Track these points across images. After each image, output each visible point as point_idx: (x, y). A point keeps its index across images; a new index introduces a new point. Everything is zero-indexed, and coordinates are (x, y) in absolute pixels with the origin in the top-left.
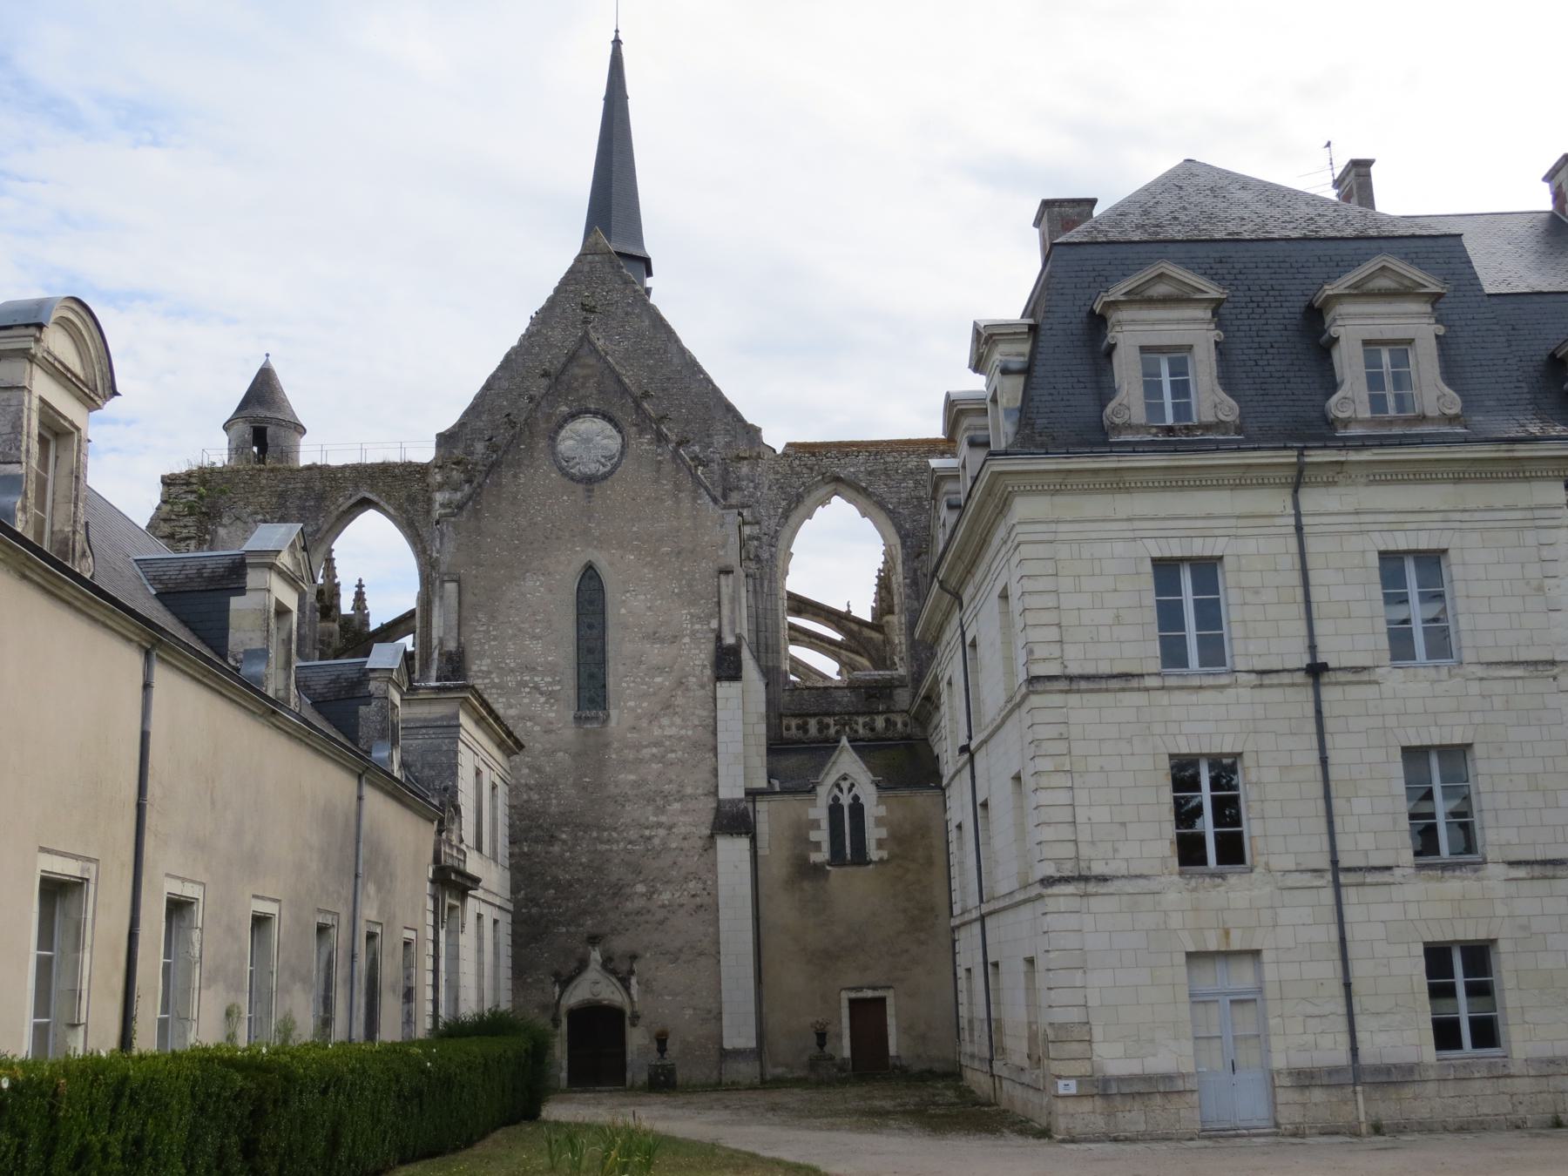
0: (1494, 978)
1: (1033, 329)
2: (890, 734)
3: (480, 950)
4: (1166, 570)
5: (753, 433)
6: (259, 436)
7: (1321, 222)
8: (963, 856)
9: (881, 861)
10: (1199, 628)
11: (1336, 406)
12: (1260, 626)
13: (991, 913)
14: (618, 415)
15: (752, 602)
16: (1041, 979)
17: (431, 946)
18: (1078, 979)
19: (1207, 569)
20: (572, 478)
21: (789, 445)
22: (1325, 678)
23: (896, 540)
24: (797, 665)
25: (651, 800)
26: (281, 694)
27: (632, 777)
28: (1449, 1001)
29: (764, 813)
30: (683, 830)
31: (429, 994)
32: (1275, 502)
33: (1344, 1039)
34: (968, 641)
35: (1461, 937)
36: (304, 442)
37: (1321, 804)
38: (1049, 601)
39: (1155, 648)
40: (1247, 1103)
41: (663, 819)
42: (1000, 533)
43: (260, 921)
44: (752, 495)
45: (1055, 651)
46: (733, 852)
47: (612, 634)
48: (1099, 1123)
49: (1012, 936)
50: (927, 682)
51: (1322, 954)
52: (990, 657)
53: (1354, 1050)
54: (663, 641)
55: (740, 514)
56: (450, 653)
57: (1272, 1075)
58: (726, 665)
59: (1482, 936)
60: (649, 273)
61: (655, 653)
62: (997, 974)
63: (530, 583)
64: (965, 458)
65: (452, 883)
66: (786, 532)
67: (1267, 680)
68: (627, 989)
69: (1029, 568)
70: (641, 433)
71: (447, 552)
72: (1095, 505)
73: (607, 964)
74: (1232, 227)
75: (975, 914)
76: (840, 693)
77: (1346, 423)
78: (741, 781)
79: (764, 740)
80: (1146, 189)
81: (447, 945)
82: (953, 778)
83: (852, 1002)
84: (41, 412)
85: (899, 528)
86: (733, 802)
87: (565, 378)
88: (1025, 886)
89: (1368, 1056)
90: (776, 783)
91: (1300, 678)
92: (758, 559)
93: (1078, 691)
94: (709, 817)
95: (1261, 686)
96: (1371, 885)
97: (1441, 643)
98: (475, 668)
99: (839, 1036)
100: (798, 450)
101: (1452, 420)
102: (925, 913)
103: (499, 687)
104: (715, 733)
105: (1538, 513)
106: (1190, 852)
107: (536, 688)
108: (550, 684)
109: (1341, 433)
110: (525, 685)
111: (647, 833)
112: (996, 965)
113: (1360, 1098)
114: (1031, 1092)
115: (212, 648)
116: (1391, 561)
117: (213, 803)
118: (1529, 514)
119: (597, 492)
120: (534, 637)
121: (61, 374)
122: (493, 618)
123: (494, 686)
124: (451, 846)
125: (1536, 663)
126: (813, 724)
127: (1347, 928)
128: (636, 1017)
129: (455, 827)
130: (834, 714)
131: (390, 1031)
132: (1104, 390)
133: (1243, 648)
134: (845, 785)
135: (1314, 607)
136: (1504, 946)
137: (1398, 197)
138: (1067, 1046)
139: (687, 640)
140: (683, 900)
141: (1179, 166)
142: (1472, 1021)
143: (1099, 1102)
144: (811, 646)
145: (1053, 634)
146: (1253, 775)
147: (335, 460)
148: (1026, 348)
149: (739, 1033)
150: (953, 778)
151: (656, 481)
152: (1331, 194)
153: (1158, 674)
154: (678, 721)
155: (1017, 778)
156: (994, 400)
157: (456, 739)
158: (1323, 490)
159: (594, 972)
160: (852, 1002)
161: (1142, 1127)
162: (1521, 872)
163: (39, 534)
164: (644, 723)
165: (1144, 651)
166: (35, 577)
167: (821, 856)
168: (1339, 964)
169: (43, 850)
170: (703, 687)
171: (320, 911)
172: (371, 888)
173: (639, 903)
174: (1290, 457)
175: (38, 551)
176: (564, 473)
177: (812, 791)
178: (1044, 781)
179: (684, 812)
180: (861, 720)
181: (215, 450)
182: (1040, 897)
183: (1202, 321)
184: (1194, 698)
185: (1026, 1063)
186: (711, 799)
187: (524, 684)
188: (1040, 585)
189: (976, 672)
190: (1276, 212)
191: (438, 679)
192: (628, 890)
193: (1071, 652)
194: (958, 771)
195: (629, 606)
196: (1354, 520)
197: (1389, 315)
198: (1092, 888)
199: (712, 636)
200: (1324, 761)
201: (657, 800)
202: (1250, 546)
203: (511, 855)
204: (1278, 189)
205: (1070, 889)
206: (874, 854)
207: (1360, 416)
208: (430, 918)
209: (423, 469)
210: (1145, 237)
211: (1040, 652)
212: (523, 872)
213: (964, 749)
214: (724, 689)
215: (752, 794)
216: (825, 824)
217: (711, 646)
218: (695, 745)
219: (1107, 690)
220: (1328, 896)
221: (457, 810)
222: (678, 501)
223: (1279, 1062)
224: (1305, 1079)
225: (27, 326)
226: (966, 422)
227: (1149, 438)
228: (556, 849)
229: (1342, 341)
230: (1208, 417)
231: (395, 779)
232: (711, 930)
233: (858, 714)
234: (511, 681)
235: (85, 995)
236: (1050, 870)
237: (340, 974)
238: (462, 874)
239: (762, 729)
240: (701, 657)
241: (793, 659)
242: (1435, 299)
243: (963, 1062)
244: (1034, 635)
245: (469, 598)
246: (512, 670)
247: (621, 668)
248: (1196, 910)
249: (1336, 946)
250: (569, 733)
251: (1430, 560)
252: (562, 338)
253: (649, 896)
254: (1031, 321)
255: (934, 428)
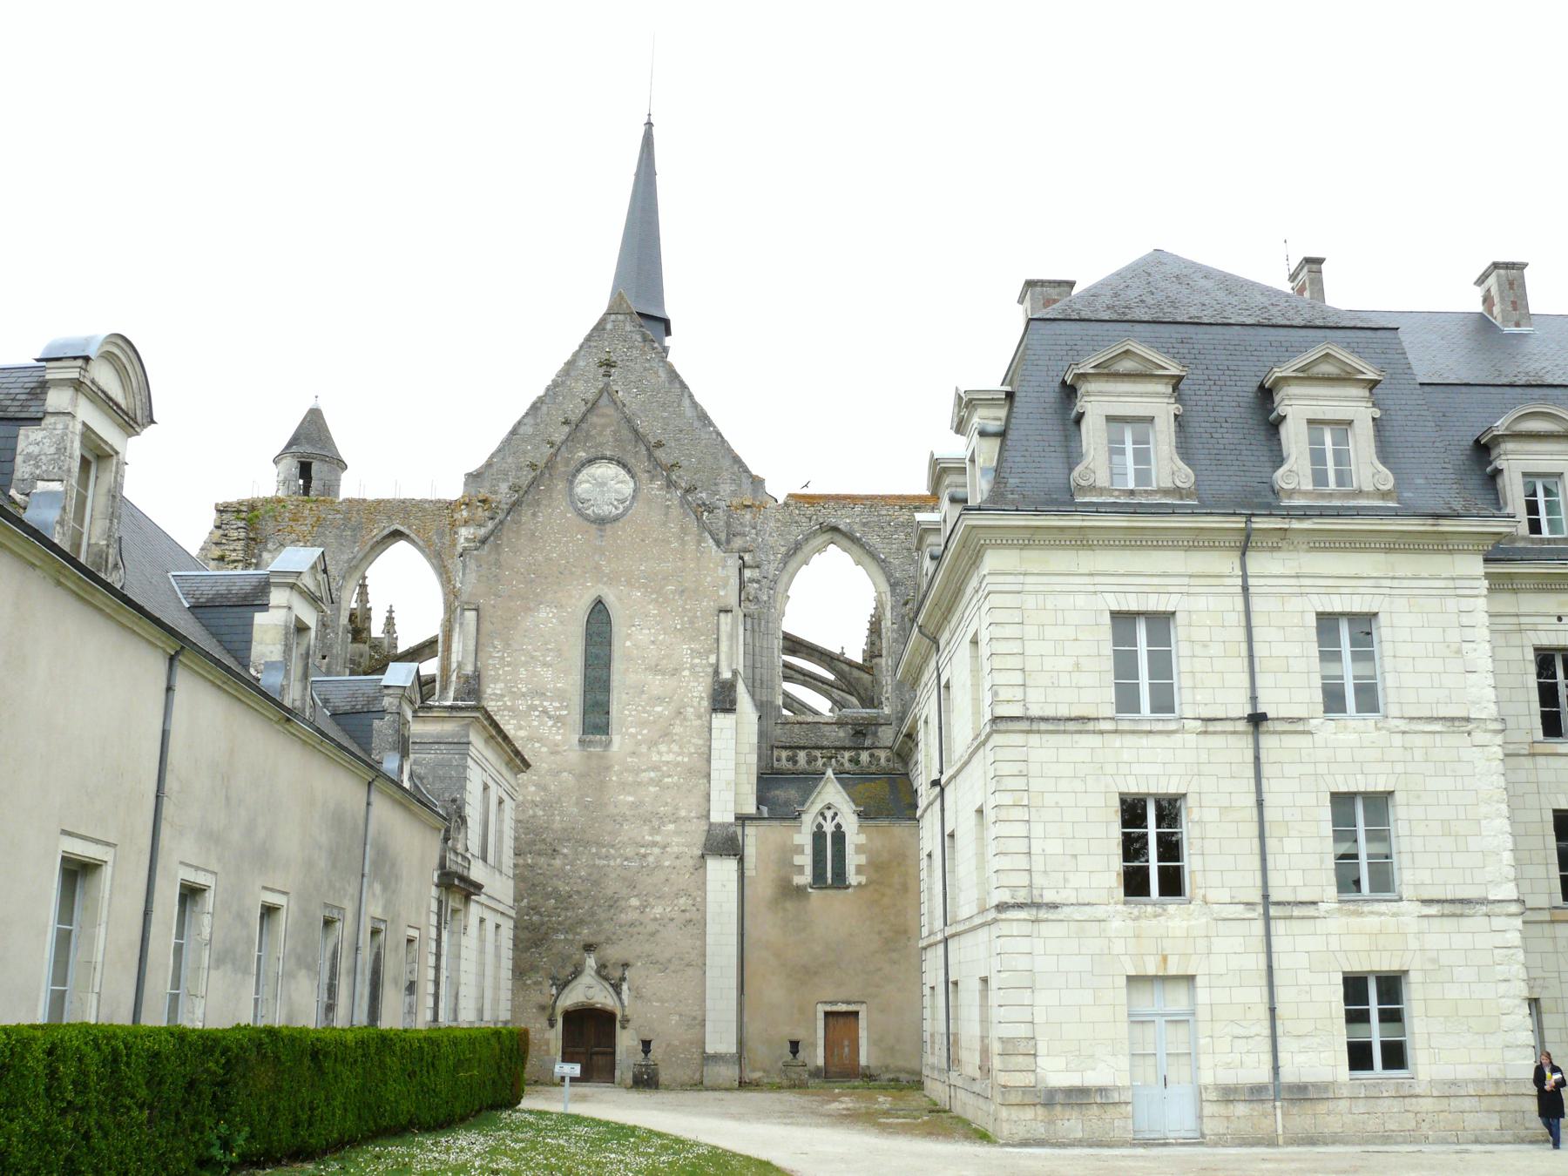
0: (1404, 1006)
1: (1010, 396)
2: (873, 769)
3: (482, 951)
4: (1123, 620)
5: (757, 483)
6: (305, 470)
7: (1274, 311)
8: (930, 882)
9: (859, 885)
10: (1151, 677)
11: (1282, 478)
12: (1208, 677)
13: (953, 936)
14: (631, 461)
15: (749, 640)
16: (994, 997)
17: (433, 945)
18: (1026, 996)
19: (1161, 622)
20: (586, 518)
21: (790, 496)
22: (1265, 726)
23: (885, 587)
24: (791, 702)
25: (646, 821)
26: (298, 704)
27: (631, 799)
28: (1364, 1026)
29: (753, 839)
30: (676, 849)
31: (431, 988)
32: (1226, 563)
33: (1267, 1058)
34: (943, 683)
35: (1376, 968)
36: (345, 477)
37: (1256, 842)
38: (1015, 647)
39: (1110, 694)
40: (1177, 1117)
41: (658, 838)
42: (974, 583)
43: (269, 911)
44: (754, 540)
45: (1018, 693)
46: (722, 872)
47: (617, 666)
48: (1040, 1131)
49: (971, 957)
50: (908, 722)
51: (1248, 977)
52: (961, 698)
53: (1276, 1069)
54: (664, 674)
55: (741, 558)
56: (467, 677)
57: (1200, 1090)
58: (723, 699)
59: (1395, 967)
60: (668, 332)
61: (656, 684)
62: (956, 992)
63: (544, 613)
64: (945, 512)
65: (456, 886)
66: (785, 578)
67: (1211, 727)
68: (619, 994)
69: (999, 616)
70: (652, 479)
71: (468, 581)
72: (1061, 560)
73: (602, 971)
74: (1194, 312)
75: (940, 937)
76: (827, 728)
77: (1291, 493)
78: (731, 806)
79: (754, 770)
80: (1118, 274)
81: (450, 945)
82: (925, 810)
83: (827, 1014)
84: (83, 435)
85: (888, 576)
86: (723, 825)
87: (584, 426)
88: (983, 911)
89: (1288, 1075)
90: (765, 809)
91: (1242, 726)
92: (757, 600)
93: (1039, 732)
94: (700, 839)
95: (1206, 732)
96: (1299, 918)
97: (1368, 698)
98: (489, 691)
99: (815, 1045)
100: (803, 500)
101: (1384, 495)
102: (898, 938)
103: (511, 709)
104: (709, 761)
105: (1459, 583)
106: (1135, 884)
107: (545, 712)
108: (556, 709)
109: (1285, 502)
110: (535, 708)
111: (643, 850)
112: (956, 983)
113: (1279, 1112)
114: (981, 1100)
115: (236, 658)
116: (1327, 622)
117: (227, 798)
118: (1451, 584)
119: (609, 532)
120: (545, 664)
121: (105, 402)
122: (507, 645)
123: (506, 708)
124: (456, 853)
125: (1453, 719)
126: (802, 755)
127: (1275, 956)
128: (626, 1021)
129: (461, 836)
130: (822, 748)
131: (392, 1019)
132: (1072, 456)
133: (1191, 698)
134: (829, 814)
135: (1257, 661)
136: (1414, 977)
137: (1345, 293)
138: (1014, 1059)
139: (686, 673)
140: (675, 914)
141: (1150, 255)
142: (1384, 1045)
143: (1040, 1110)
144: (804, 684)
145: (1017, 678)
146: (1195, 815)
147: (371, 495)
148: (1003, 413)
149: (721, 1040)
150: (925, 810)
151: (664, 524)
152: (1287, 287)
153: (1112, 719)
154: (675, 748)
155: (980, 811)
156: (972, 460)
157: (466, 755)
158: (1268, 554)
159: (588, 978)
160: (827, 1014)
161: (1079, 1135)
162: (1434, 910)
163: (77, 546)
164: (644, 749)
165: (1099, 696)
166: (69, 584)
167: (806, 878)
168: (1265, 990)
169: (65, 832)
170: (700, 717)
171: (326, 905)
172: (377, 887)
173: (633, 915)
174: (1238, 523)
175: (73, 562)
176: (580, 513)
177: (797, 817)
178: (1003, 814)
179: (677, 833)
180: (847, 755)
181: (264, 480)
182: (995, 921)
183: (1163, 395)
184: (1144, 741)
185: (977, 1074)
186: (703, 822)
187: (533, 708)
188: (1008, 631)
189: (948, 711)
190: (1234, 300)
191: (455, 699)
192: (622, 903)
193: (1034, 695)
194: (930, 804)
195: (634, 639)
196: (1299, 586)
197: (1332, 398)
198: (1043, 914)
199: (710, 670)
200: (1260, 804)
201: (654, 820)
202: (1200, 603)
203: (516, 866)
204: (1236, 279)
205: (1022, 914)
206: (853, 878)
207: (1304, 487)
208: (434, 919)
209: (451, 506)
210: (1115, 317)
211: (1004, 694)
212: (527, 883)
213: (935, 783)
214: (720, 720)
215: (742, 819)
216: (809, 850)
217: (709, 680)
218: (691, 771)
219: (1065, 732)
220: (1258, 927)
221: (463, 820)
222: (683, 543)
223: (1207, 1078)
224: (1228, 1094)
225: (75, 358)
226: (948, 480)
227: (1112, 500)
228: (558, 862)
229: (1289, 418)
230: (1167, 483)
231: (404, 789)
232: (698, 943)
233: (844, 748)
234: (522, 705)
235: (99, 968)
236: (1005, 896)
237: (344, 965)
238: (464, 879)
239: (753, 759)
240: (699, 691)
241: (786, 695)
242: (1373, 384)
243: (926, 1072)
244: (1000, 678)
245: (486, 626)
246: (524, 695)
247: (624, 696)
248: (1137, 937)
249: (1264, 974)
250: (574, 755)
251: (1364, 624)
252: (585, 388)
253: (642, 909)
254: (1008, 389)
255: (921, 487)
